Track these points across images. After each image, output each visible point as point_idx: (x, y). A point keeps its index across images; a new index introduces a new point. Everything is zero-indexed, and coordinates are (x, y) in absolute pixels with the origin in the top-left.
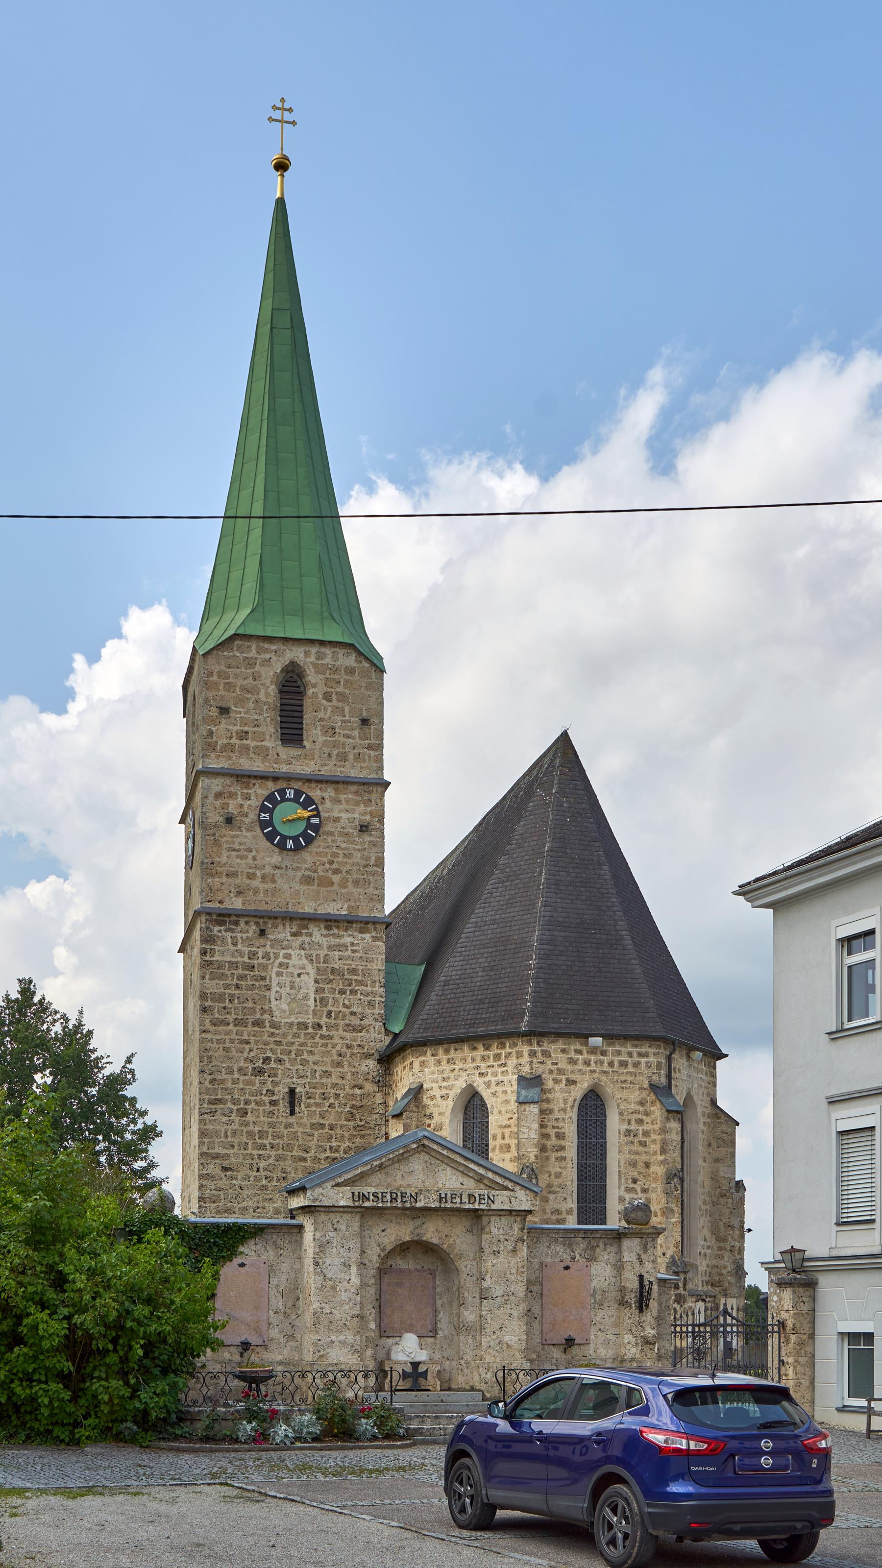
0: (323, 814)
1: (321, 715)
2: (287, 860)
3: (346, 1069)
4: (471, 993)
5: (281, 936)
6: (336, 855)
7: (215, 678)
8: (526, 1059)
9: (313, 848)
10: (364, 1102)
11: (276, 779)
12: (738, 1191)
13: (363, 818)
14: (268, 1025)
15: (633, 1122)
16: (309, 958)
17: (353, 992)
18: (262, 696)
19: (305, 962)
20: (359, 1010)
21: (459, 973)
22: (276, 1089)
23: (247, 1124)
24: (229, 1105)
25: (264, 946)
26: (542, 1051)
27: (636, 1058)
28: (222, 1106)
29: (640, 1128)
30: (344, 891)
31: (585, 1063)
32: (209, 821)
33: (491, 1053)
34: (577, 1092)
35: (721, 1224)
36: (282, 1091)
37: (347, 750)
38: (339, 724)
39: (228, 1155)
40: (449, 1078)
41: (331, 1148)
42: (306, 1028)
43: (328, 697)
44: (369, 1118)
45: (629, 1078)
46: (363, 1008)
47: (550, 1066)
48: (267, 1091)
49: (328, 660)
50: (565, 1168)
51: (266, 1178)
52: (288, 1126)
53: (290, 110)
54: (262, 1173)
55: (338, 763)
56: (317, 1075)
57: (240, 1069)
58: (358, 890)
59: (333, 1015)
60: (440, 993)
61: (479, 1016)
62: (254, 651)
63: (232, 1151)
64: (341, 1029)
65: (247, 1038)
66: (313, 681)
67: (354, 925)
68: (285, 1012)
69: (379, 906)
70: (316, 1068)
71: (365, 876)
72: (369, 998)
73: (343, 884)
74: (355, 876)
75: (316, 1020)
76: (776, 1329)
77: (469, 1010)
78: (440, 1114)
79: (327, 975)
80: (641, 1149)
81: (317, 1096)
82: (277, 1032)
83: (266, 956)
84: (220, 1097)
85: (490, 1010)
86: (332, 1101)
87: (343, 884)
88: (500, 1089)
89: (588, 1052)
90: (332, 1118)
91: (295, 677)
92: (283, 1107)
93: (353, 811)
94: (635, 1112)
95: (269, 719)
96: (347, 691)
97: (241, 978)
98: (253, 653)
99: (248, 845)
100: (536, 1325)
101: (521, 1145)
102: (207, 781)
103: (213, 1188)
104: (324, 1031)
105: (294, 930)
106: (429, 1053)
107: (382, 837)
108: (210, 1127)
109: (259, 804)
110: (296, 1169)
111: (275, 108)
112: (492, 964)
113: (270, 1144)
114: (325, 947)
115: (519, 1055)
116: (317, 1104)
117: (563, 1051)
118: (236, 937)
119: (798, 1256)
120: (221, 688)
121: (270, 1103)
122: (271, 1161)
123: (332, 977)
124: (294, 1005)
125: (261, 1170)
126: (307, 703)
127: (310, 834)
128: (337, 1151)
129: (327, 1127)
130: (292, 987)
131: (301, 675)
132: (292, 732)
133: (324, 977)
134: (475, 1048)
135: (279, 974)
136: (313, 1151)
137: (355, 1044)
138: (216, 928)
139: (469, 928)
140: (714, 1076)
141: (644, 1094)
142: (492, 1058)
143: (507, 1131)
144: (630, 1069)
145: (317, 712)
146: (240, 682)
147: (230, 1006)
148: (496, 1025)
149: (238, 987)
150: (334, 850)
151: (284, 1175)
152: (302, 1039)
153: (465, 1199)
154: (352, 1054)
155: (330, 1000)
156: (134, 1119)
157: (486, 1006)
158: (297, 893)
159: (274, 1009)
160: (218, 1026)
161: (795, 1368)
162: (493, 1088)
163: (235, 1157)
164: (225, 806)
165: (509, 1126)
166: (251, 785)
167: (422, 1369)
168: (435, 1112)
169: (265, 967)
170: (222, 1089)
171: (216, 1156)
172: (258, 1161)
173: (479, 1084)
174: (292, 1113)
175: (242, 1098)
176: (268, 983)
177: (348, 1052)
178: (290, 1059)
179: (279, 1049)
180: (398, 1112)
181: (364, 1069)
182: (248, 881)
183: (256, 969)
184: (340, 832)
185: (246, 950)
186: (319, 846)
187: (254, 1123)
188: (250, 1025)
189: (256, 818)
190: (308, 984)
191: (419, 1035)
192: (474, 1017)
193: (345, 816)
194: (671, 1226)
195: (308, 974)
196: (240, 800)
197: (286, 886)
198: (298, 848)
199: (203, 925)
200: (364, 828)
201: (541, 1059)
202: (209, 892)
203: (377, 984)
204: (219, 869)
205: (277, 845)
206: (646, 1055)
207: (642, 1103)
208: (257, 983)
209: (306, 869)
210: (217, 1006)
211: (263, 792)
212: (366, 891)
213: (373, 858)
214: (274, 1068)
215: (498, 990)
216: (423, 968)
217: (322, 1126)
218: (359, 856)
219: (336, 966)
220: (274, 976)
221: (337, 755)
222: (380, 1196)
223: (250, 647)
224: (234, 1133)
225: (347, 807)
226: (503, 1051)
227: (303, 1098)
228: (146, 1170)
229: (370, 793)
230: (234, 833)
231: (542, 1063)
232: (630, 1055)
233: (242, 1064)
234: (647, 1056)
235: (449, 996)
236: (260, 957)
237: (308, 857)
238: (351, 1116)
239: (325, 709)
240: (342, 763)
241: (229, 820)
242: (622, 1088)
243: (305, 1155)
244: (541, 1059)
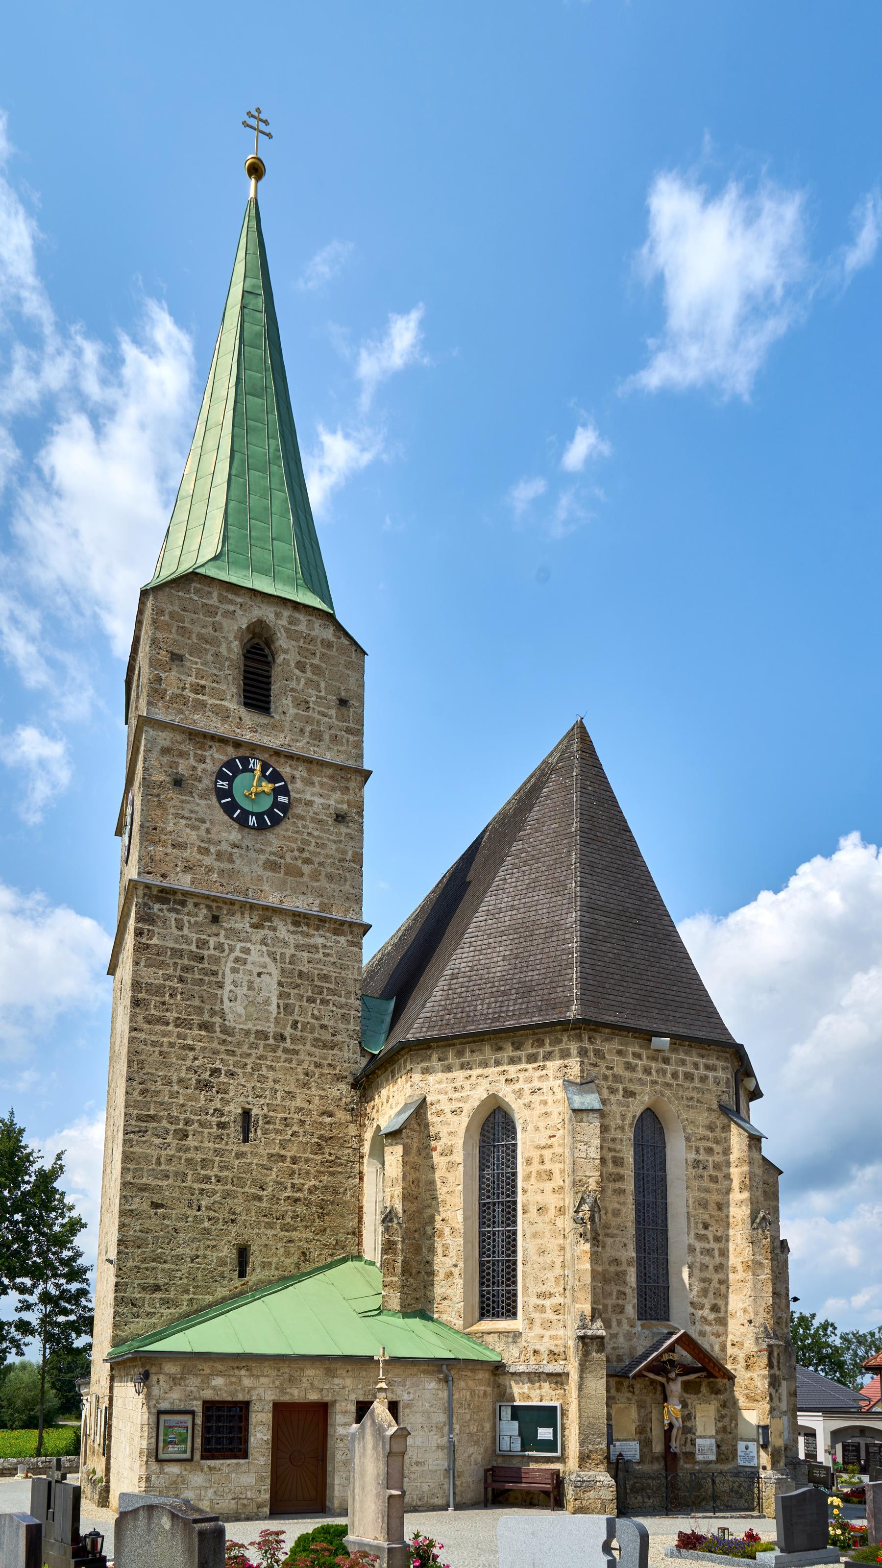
0: (293, 794)
1: (293, 684)
2: (249, 839)
3: (314, 1091)
4: (489, 985)
5: (239, 926)
6: (308, 843)
9: (280, 830)
10: (335, 1132)
11: (237, 744)
12: (782, 1252)
13: (340, 806)
14: (218, 1029)
15: (702, 1151)
16: (272, 955)
17: (324, 1002)
18: (223, 650)
19: (267, 960)
20: (331, 1023)
21: (470, 964)
22: (227, 1109)
23: (188, 1149)
24: (164, 1123)
25: (218, 935)
26: (594, 1050)
27: (702, 1071)
28: (155, 1124)
29: (710, 1159)
30: (316, 884)
31: (645, 1070)
32: (153, 778)
33: (523, 1054)
34: (636, 1108)
36: (234, 1110)
37: (322, 729)
38: (314, 699)
39: (161, 1187)
40: (462, 1087)
41: (293, 1186)
42: (267, 1038)
44: (340, 1153)
45: (696, 1095)
46: (336, 1021)
47: (604, 1070)
48: (215, 1110)
49: (302, 627)
50: (624, 1203)
51: (209, 1219)
52: (240, 1155)
53: (266, 122)
54: (203, 1213)
55: (311, 741)
56: (279, 1095)
57: (180, 1081)
58: (332, 886)
59: (299, 1025)
60: (446, 988)
61: (504, 1009)
62: (215, 599)
63: (165, 1183)
64: (308, 1044)
65: (191, 1042)
66: (285, 646)
67: (327, 925)
68: (240, 1016)
69: (356, 907)
70: (277, 1087)
71: (341, 872)
72: (343, 1011)
73: (315, 876)
74: (329, 869)
75: (278, 1030)
77: (489, 1003)
78: (450, 1134)
79: (293, 979)
81: (278, 1121)
82: (230, 1039)
83: (219, 947)
84: (152, 1112)
85: (520, 1001)
86: (295, 1128)
88: (536, 1098)
89: (648, 1058)
90: (295, 1148)
91: (263, 645)
92: (234, 1131)
93: (328, 797)
94: (704, 1138)
95: (230, 678)
96: (324, 665)
97: (186, 969)
98: (214, 601)
99: (201, 814)
101: (577, 1166)
102: (151, 732)
103: (138, 1228)
104: (288, 1044)
105: (254, 921)
106: (435, 1057)
107: (361, 831)
108: (137, 1149)
109: (216, 769)
110: (248, 1210)
111: (250, 114)
112: (515, 951)
113: (216, 1176)
114: (292, 946)
116: (277, 1132)
117: (620, 1053)
118: (182, 920)
120: (173, 631)
121: (218, 1125)
122: (217, 1197)
123: (299, 981)
124: (252, 1009)
125: (203, 1209)
126: (276, 672)
127: (274, 817)
128: (300, 1190)
129: (288, 1159)
130: (250, 988)
131: (269, 641)
132: (257, 694)
133: (289, 980)
134: (500, 1049)
135: (234, 970)
136: (270, 1189)
137: (325, 1062)
138: (157, 906)
139: (480, 916)
141: (713, 1117)
142: (524, 1059)
143: (547, 1153)
145: (288, 683)
146: (197, 629)
147: (172, 1001)
148: (532, 1017)
149: (181, 980)
150: (305, 837)
151: (233, 1217)
152: (260, 1051)
154: (322, 1075)
155: (297, 1008)
156: (63, 1213)
157: (514, 997)
158: (260, 879)
159: (227, 1011)
160: (155, 1024)
162: (527, 1098)
163: (169, 1189)
164: (173, 765)
165: (551, 1146)
166: (208, 748)
168: (444, 1131)
169: (217, 960)
170: (155, 1102)
171: (144, 1188)
172: (200, 1197)
173: (506, 1093)
174: (246, 1140)
175: (182, 1117)
176: (220, 979)
177: (317, 1071)
178: (244, 1073)
179: (231, 1060)
180: (397, 1127)
181: (334, 1093)
182: (199, 857)
183: (206, 961)
184: (312, 818)
185: (194, 937)
186: (287, 830)
187: (196, 1148)
188: (195, 1027)
189: (211, 786)
190: (270, 985)
191: (422, 1034)
192: (498, 1010)
193: (318, 800)
194: (760, 1284)
195: (270, 974)
196: (192, 761)
197: (246, 869)
198: (262, 827)
199: (140, 900)
200: (340, 818)
201: (593, 1059)
202: (148, 865)
203: (353, 996)
204: (163, 837)
205: (236, 820)
206: (713, 1068)
207: (711, 1128)
208: (206, 978)
209: (272, 853)
210: (154, 1000)
211: (221, 757)
212: (342, 888)
213: (350, 853)
214: (224, 1083)
215: (527, 979)
216: (392, 1004)
217: (283, 1158)
218: (334, 848)
219: (305, 969)
220: (228, 971)
221: (311, 733)
223: (210, 593)
224: (170, 1159)
225: (321, 791)
226: (541, 1050)
227: (260, 1122)
228: (73, 1259)
229: (348, 780)
230: (184, 798)
232: (696, 1066)
233: (183, 1075)
234: (715, 1070)
235: (459, 990)
236: (212, 947)
237: (274, 840)
238: (319, 1148)
239: (298, 679)
240: (316, 742)
242: (688, 1106)
243: (261, 1193)
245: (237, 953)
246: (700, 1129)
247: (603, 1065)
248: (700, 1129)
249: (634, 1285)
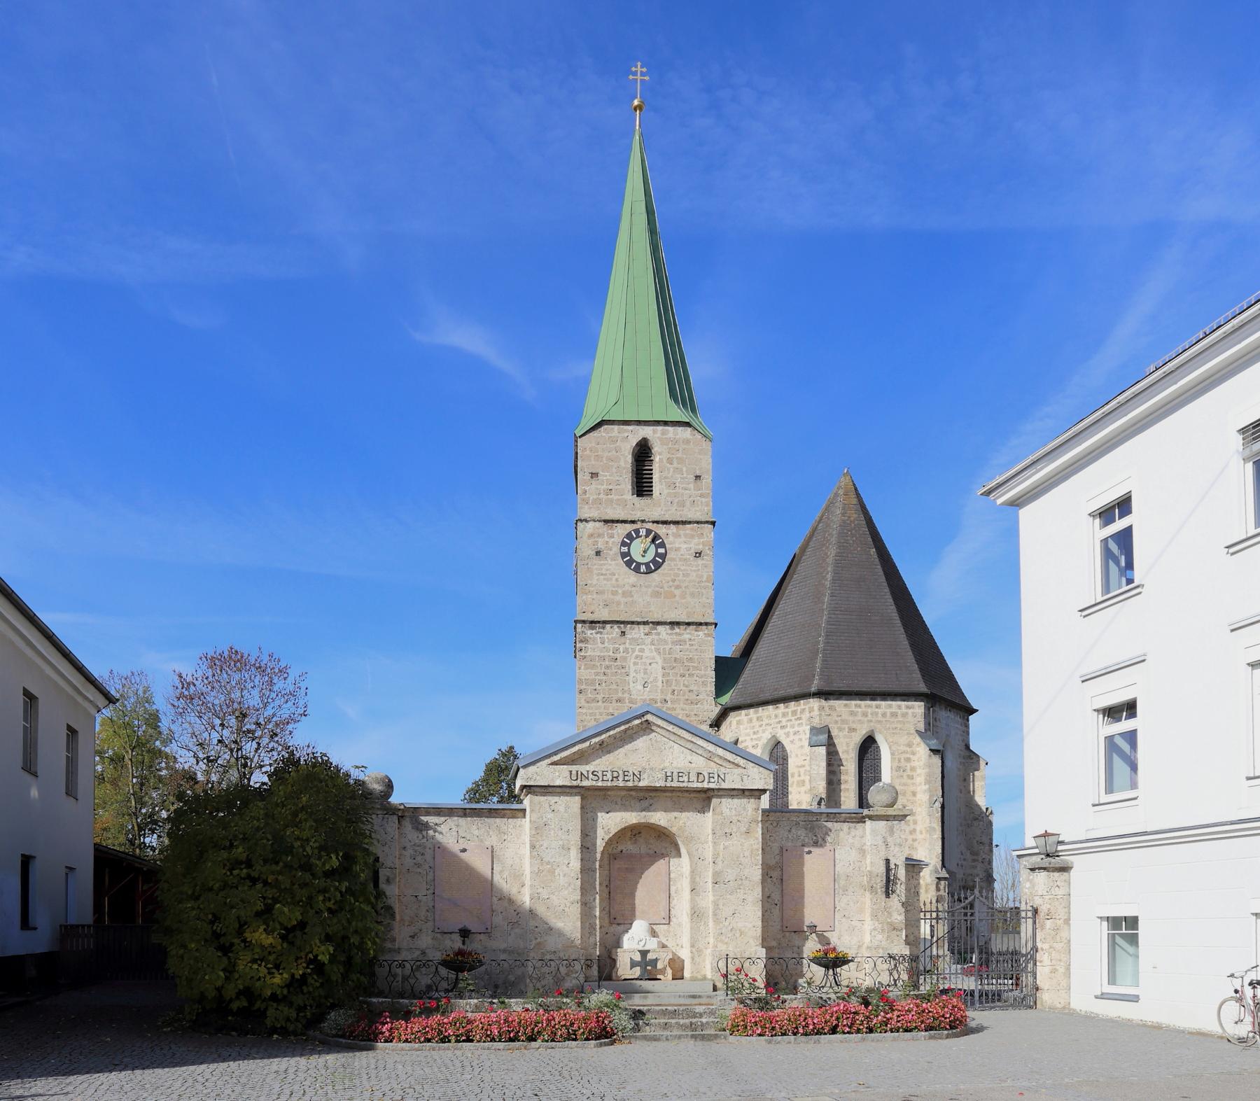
6: (678, 575)
7: (588, 452)
8: (816, 712)
11: (633, 522)
16: (658, 651)
27: (904, 710)
43: (670, 461)
73: (683, 596)
76: (1030, 914)
80: (910, 781)
83: (626, 651)
87: (683, 596)
88: (796, 737)
97: (607, 667)
100: (776, 911)
115: (811, 710)
119: (1051, 840)
127: (656, 565)
130: (645, 673)
132: (642, 486)
135: (635, 664)
140: (967, 726)
143: (802, 770)
146: (606, 454)
153: (693, 778)
161: (1050, 954)
167: (650, 956)
169: (625, 659)
190: (657, 670)
198: (649, 571)
201: (828, 712)
210: (590, 688)
222: (600, 774)
241: (598, 553)
244: (828, 712)
245: (637, 653)
247: (834, 714)
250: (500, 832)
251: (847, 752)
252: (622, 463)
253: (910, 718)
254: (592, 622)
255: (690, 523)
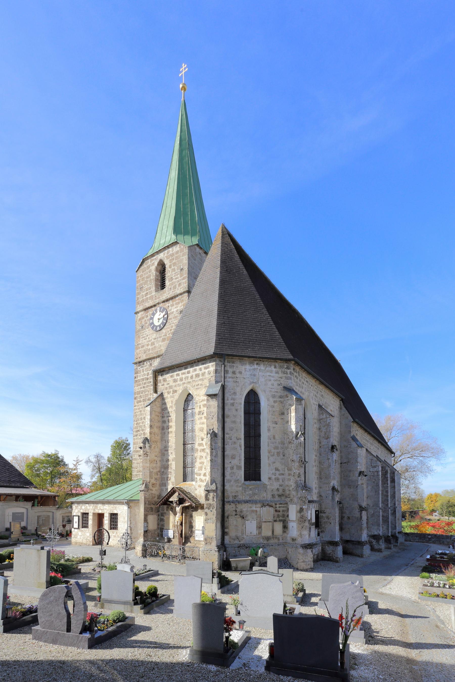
15: (202, 407)
24: (141, 432)
35: (290, 460)
45: (200, 382)
97: (145, 383)
144: (201, 377)
151: (282, 400)
206: (208, 368)
231: (163, 385)
232: (201, 369)
242: (197, 389)
246: (202, 397)
248: (202, 397)
249: (174, 469)
250: (390, 430)
251: (171, 407)
252: (152, 278)
253: (207, 376)
254: (140, 362)
255: (177, 296)
